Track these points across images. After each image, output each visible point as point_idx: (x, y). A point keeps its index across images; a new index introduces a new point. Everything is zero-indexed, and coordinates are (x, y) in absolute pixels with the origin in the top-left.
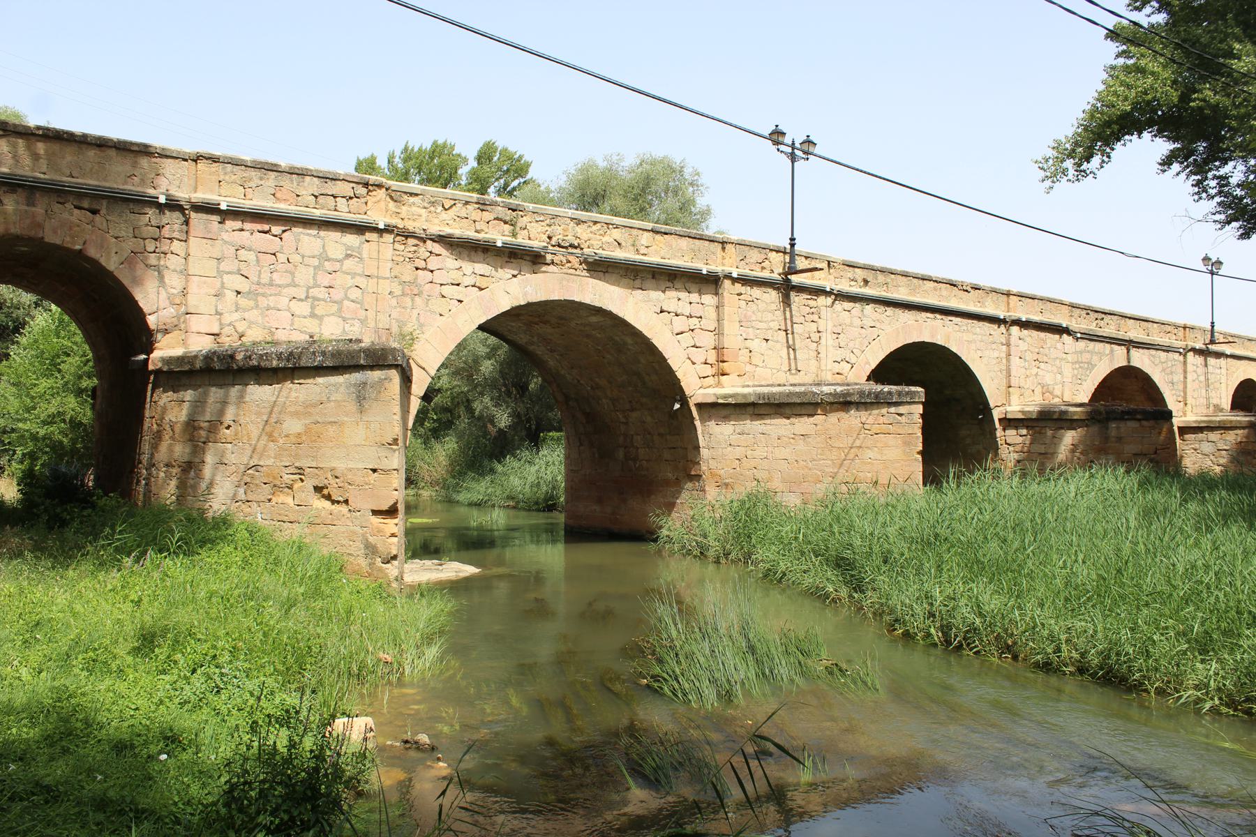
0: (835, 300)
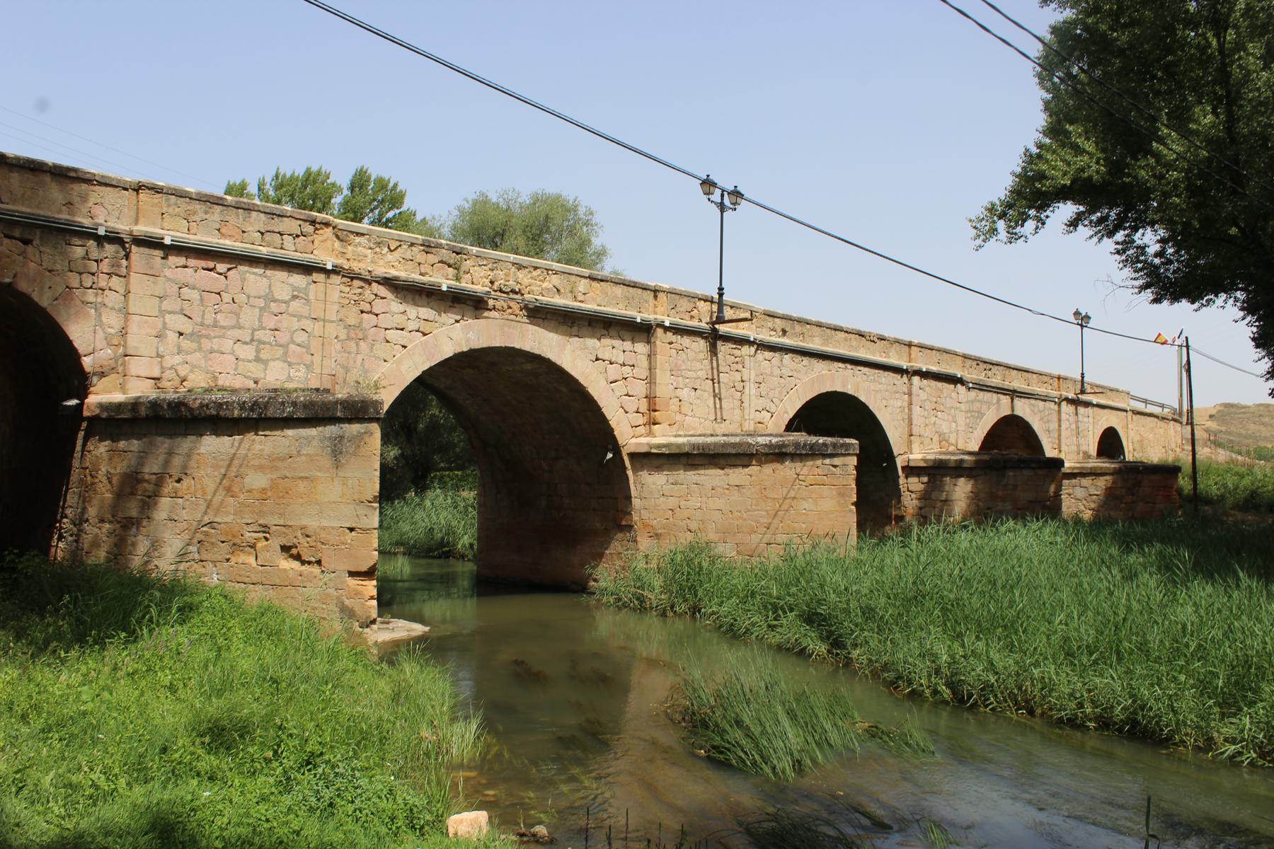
0: (757, 350)
